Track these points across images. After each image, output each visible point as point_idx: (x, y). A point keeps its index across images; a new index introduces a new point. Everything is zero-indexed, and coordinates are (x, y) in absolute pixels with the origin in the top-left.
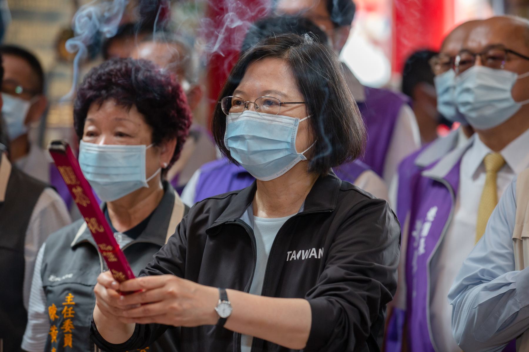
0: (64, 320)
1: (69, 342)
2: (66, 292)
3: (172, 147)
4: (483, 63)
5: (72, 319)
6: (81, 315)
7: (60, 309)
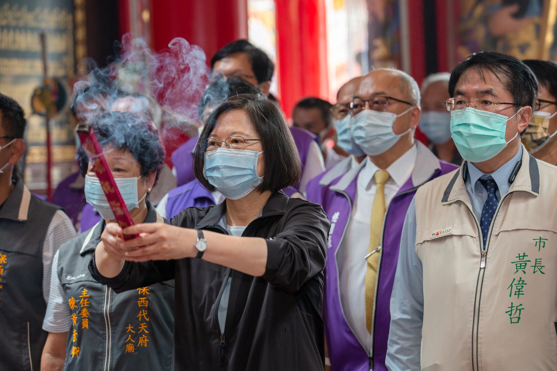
0: (82, 308)
1: (86, 324)
2: (82, 288)
3: (153, 178)
4: (371, 107)
5: (88, 308)
6: (94, 304)
7: (78, 301)
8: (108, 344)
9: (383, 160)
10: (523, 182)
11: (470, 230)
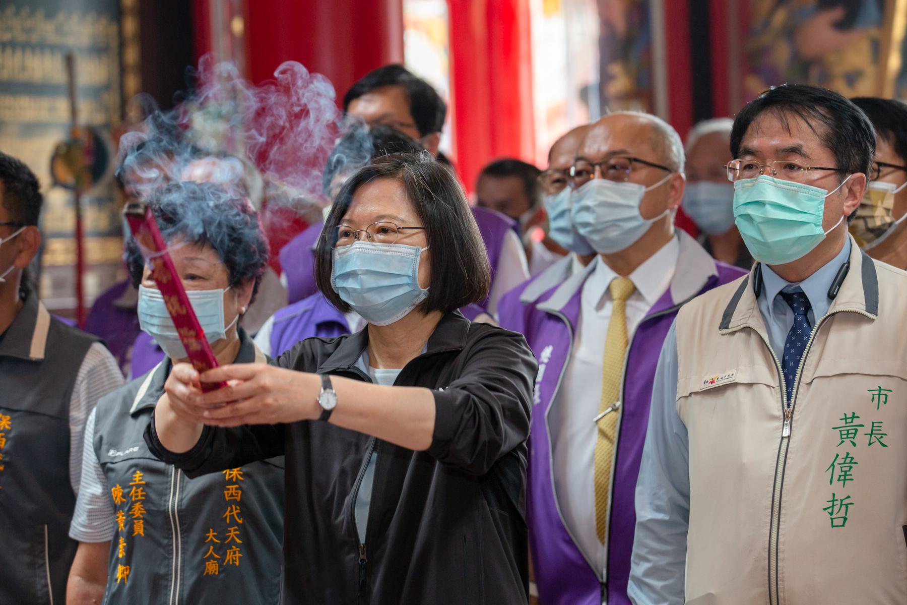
0: (133, 503)
1: (139, 529)
2: (133, 469)
3: (249, 290)
4: (604, 175)
5: (143, 502)
6: (153, 496)
7: (127, 490)
8: (177, 561)
9: (624, 262)
10: (852, 296)
11: (765, 374)
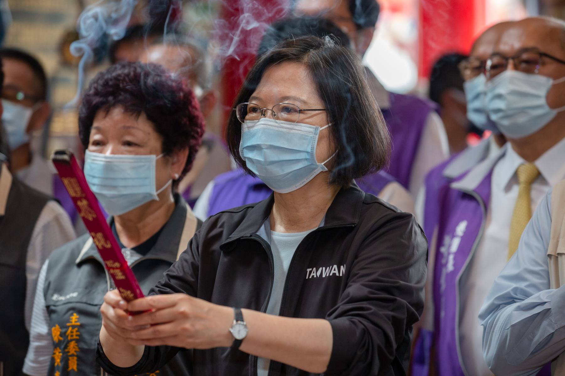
0: (69, 342)
1: (73, 365)
2: (71, 312)
3: (183, 157)
4: (516, 68)
5: (77, 341)
6: (86, 336)
7: (64, 330)
